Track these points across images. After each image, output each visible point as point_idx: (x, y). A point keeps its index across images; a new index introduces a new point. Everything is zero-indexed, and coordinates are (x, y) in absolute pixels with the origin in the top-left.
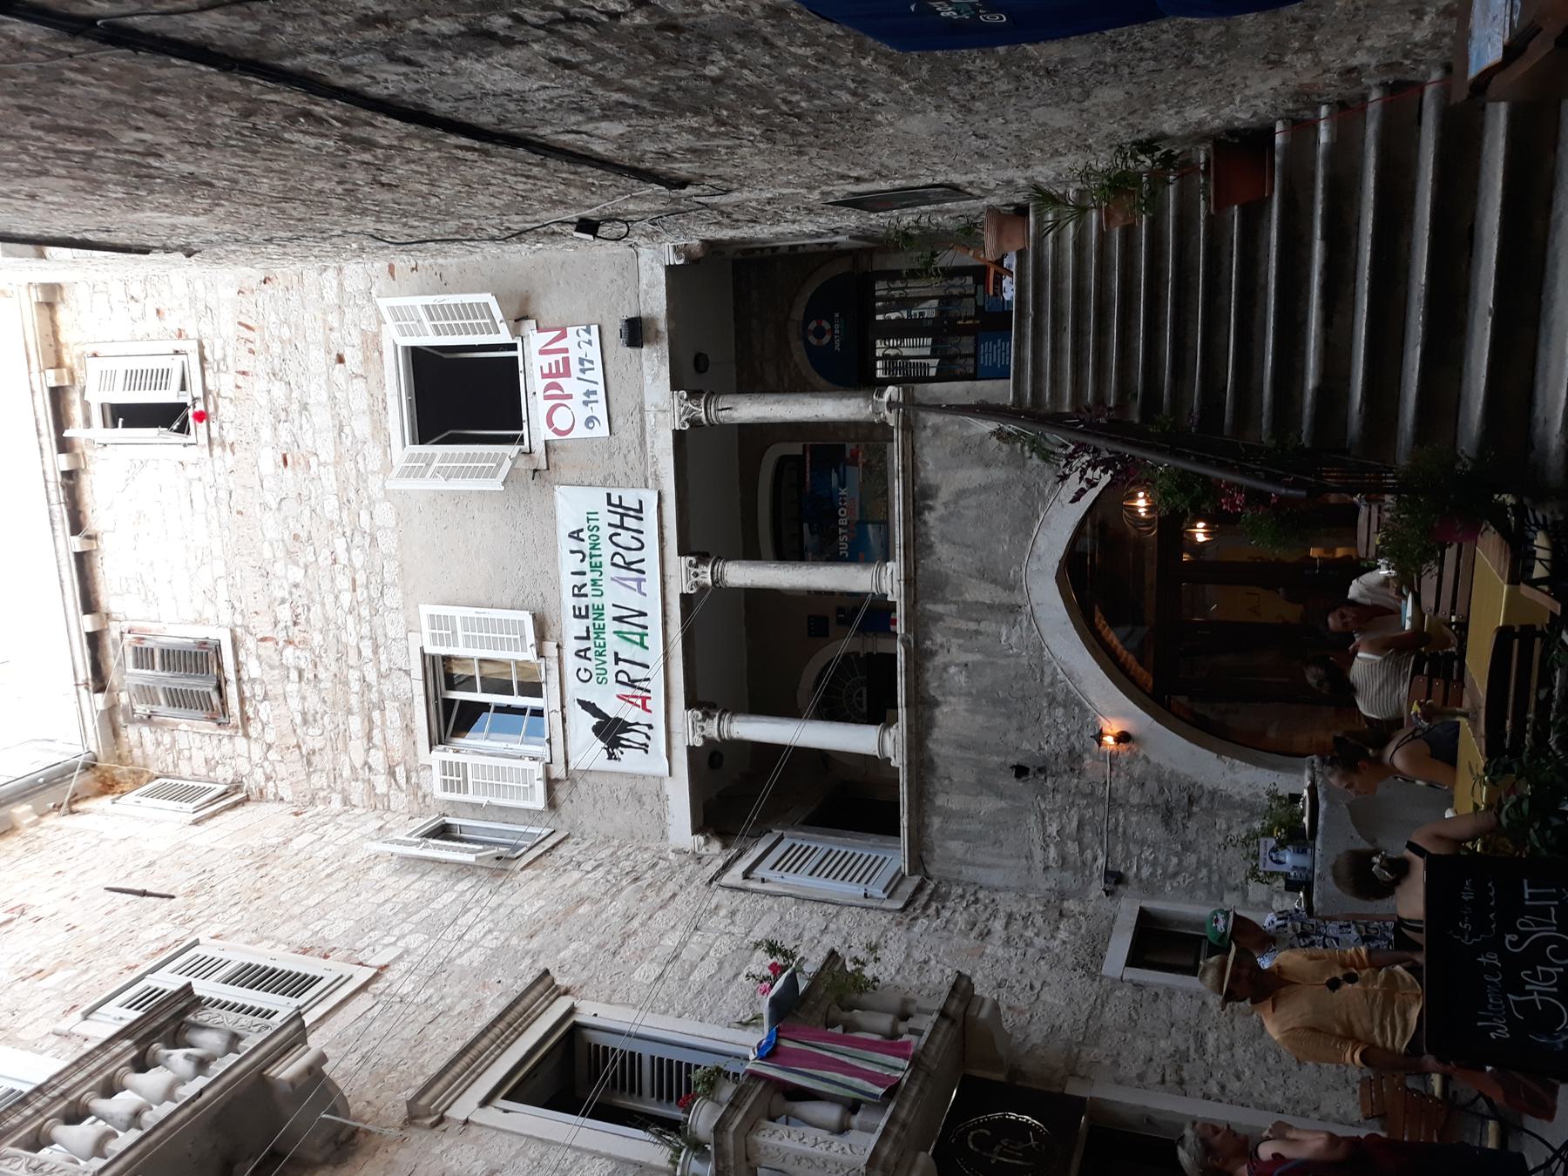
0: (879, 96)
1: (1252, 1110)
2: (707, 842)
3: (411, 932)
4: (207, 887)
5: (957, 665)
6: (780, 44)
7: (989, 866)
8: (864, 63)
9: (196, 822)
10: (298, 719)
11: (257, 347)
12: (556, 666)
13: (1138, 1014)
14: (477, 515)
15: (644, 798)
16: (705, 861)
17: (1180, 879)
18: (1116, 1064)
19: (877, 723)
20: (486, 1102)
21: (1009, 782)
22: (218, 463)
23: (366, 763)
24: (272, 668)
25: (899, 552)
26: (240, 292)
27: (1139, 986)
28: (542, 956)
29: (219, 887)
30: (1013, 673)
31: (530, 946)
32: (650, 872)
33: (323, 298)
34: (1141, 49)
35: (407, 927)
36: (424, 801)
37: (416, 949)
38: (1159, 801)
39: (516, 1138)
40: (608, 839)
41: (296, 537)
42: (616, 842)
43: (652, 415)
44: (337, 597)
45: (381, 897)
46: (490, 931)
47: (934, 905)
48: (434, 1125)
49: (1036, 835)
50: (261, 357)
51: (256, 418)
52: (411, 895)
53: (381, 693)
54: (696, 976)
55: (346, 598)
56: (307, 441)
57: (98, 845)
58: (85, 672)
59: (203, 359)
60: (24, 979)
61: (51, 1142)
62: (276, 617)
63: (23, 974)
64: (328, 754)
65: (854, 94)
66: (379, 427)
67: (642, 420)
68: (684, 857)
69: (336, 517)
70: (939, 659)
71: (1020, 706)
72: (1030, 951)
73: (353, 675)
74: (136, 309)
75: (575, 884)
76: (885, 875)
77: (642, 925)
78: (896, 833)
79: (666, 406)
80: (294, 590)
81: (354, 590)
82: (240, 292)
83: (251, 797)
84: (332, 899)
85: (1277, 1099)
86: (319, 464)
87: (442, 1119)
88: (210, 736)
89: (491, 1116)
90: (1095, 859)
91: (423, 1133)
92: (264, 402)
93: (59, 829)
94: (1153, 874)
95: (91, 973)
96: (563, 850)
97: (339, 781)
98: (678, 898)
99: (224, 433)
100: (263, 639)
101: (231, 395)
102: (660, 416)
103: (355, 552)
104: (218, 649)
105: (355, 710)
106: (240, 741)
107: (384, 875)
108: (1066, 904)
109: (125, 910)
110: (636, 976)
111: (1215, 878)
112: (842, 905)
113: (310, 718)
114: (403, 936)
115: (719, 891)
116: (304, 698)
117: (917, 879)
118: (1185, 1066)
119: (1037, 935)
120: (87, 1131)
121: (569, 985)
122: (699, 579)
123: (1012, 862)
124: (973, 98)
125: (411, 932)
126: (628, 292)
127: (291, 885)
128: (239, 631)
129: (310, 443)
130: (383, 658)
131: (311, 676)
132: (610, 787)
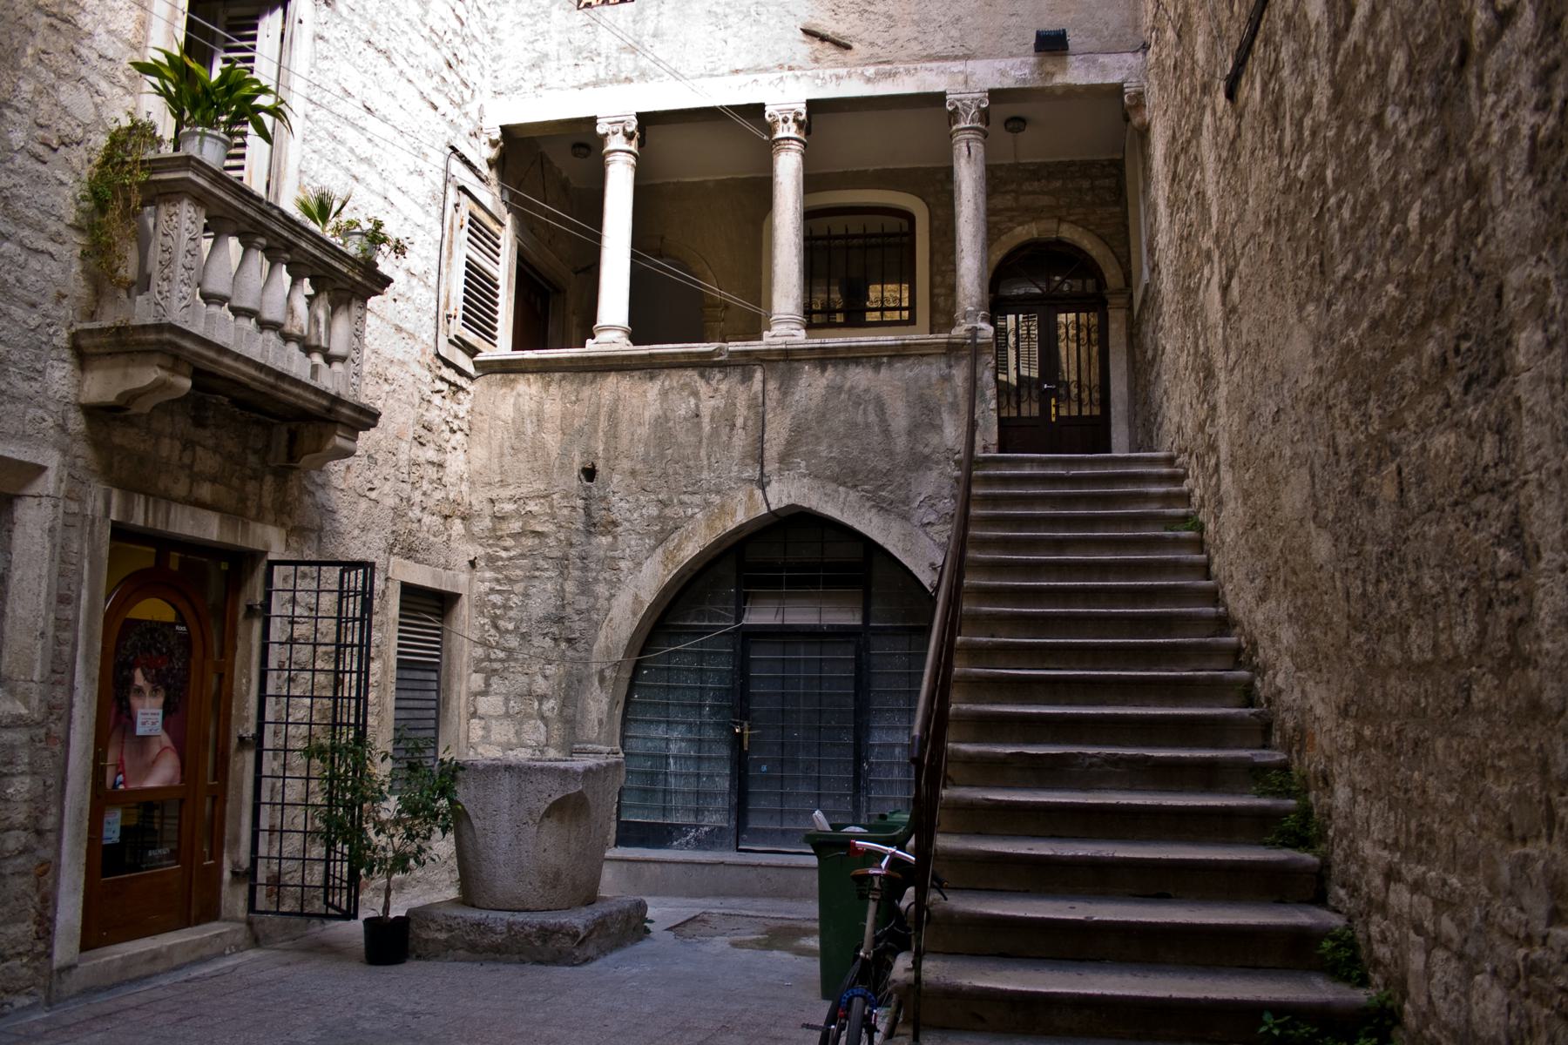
0: (1340, 307)
2: (493, 144)
5: (697, 406)
6: (1427, 191)
8: (1390, 288)
15: (537, 71)
16: (473, 140)
17: (493, 632)
19: (630, 324)
21: (577, 463)
25: (816, 343)
30: (691, 463)
32: (457, 81)
34: (1378, 581)
38: (569, 610)
43: (961, 67)
47: (445, 387)
49: (524, 490)
65: (1346, 278)
67: (956, 58)
70: (701, 385)
71: (658, 472)
72: (408, 487)
78: (514, 349)
90: (506, 549)
94: (494, 606)
98: (433, 111)
102: (961, 78)
108: (458, 521)
111: (497, 665)
117: (471, 369)
119: (424, 494)
122: (781, 124)
123: (495, 467)
124: (1329, 408)
132: (548, 32)
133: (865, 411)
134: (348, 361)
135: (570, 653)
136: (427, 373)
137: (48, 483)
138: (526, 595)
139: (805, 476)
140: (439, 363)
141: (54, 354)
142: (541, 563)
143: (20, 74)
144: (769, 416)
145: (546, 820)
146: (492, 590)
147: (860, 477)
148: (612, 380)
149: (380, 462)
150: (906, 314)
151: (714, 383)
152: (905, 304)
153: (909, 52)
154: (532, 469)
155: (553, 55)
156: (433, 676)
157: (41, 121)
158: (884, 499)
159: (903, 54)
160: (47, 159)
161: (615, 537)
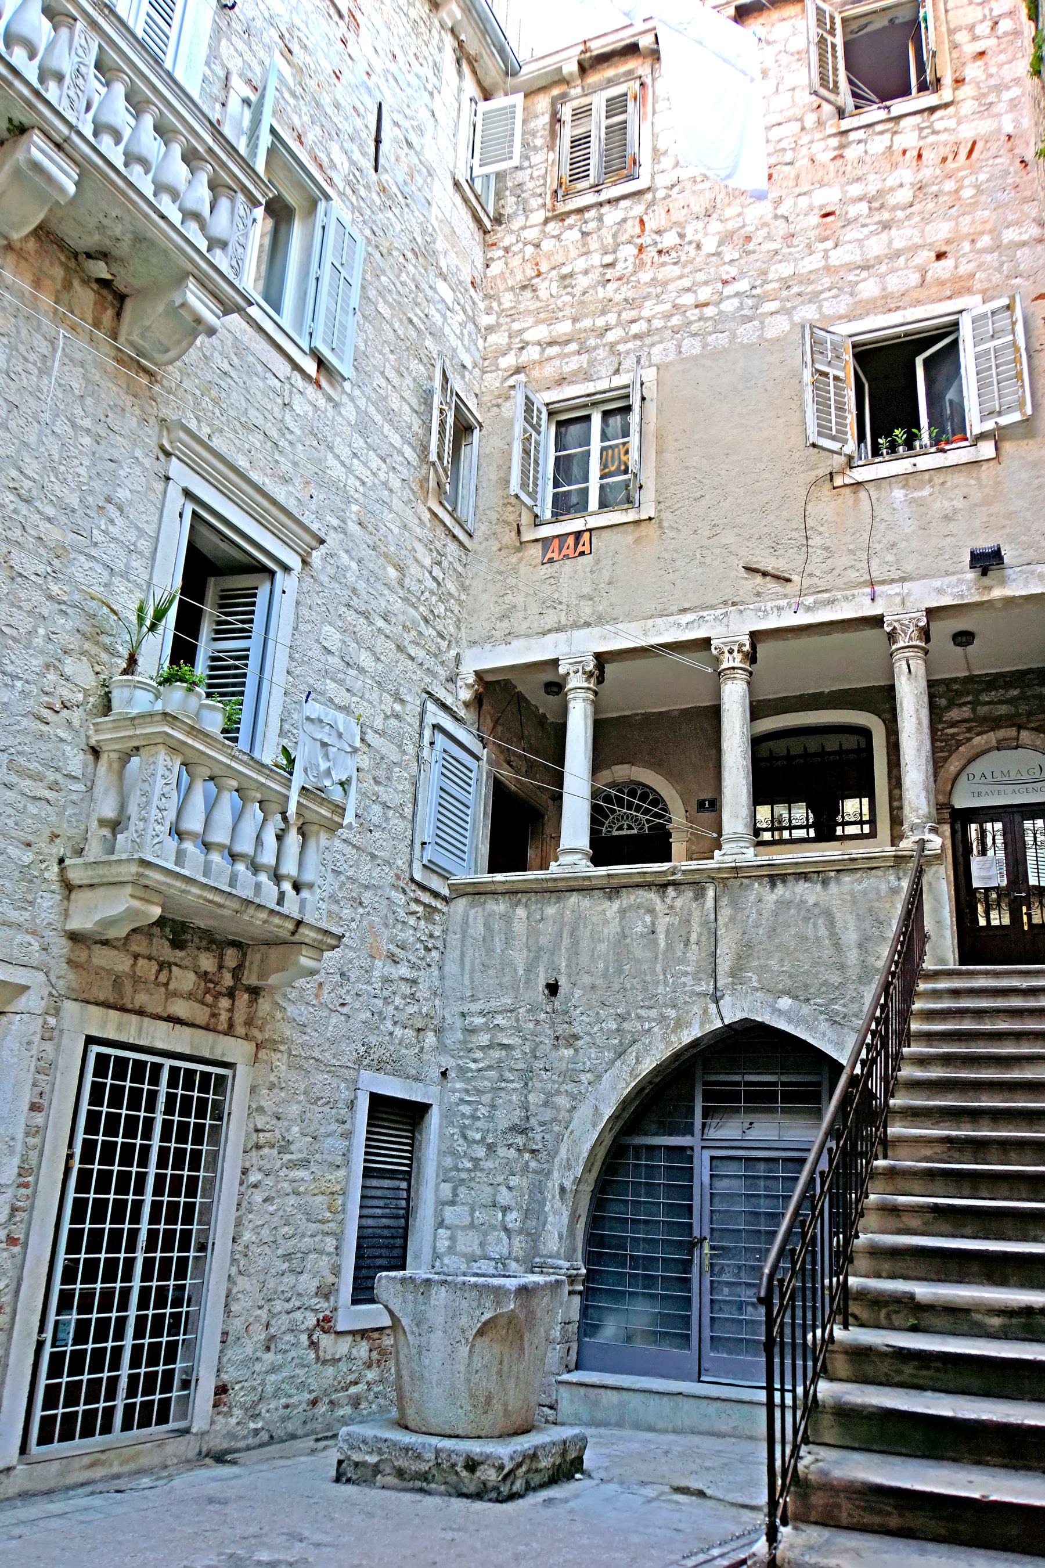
1: (234, 1214)
2: (469, 686)
3: (357, 407)
4: (389, 203)
5: (653, 923)
7: (462, 960)
9: (457, 184)
10: (565, 270)
11: (950, 165)
12: (631, 519)
13: (323, 1105)
14: (782, 420)
16: (450, 686)
17: (461, 1141)
18: (272, 1087)
20: (188, 494)
22: (821, 145)
23: (527, 343)
24: (615, 236)
26: (1010, 137)
27: (352, 1105)
28: (342, 536)
29: (390, 214)
30: (648, 978)
31: (350, 523)
32: (434, 633)
33: (1008, 227)
35: (362, 403)
36: (493, 406)
37: (340, 413)
39: (155, 526)
40: (464, 588)
41: (748, 239)
42: (463, 597)
43: (898, 590)
44: (689, 290)
45: (391, 374)
46: (363, 483)
47: (420, 909)
48: (162, 448)
50: (938, 171)
51: (871, 177)
52: (395, 403)
53: (595, 348)
54: (331, 685)
55: (688, 299)
56: (853, 234)
57: (425, 89)
58: (598, 47)
59: (932, 110)
60: (282, 37)
61: (108, 84)
62: (665, 231)
63: (287, 36)
64: (533, 305)
66: (869, 307)
67: (893, 581)
68: (452, 665)
69: (771, 276)
70: (659, 907)
71: (616, 987)
72: (379, 1003)
73: (612, 318)
74: (984, 29)
75: (417, 561)
76: (444, 861)
77: (379, 630)
78: (492, 870)
79: (908, 604)
80: (694, 245)
81: (697, 306)
82: (1010, 137)
83: (488, 236)
84: (386, 327)
85: (247, 1236)
86: (826, 251)
87: (168, 454)
88: (544, 185)
89: (175, 500)
90: (475, 1061)
91: (155, 439)
92: (890, 182)
93: (440, 50)
94: (463, 1115)
95: (292, 101)
96: (452, 547)
97: (508, 320)
98: (410, 662)
99: (854, 145)
100: (642, 222)
101: (895, 147)
102: (898, 599)
103: (736, 302)
104: (631, 177)
105: (578, 326)
106: (539, 216)
107: (414, 374)
108: (431, 1034)
109: (359, 123)
110: (327, 629)
111: (464, 1175)
112: (413, 821)
113: (568, 281)
114: (352, 399)
115: (418, 703)
116: (586, 272)
117: (446, 892)
118: (275, 1151)
119: (396, 1008)
120: (120, 114)
121: (314, 565)
123: (467, 982)
125: (357, 407)
126: (1031, 552)
127: (398, 285)
128: (649, 196)
129: (847, 238)
130: (630, 345)
131: (608, 277)
133: (815, 925)
134: (316, 887)
135: (533, 1164)
136: (401, 896)
137: (33, 1001)
138: (493, 1107)
139: (757, 990)
140: (414, 887)
141: (44, 887)
142: (508, 1075)
143: (31, 652)
144: (721, 932)
145: (479, 1340)
146: (461, 1100)
147: (812, 990)
148: (574, 899)
149: (352, 979)
150: (866, 829)
151: (668, 900)
152: (866, 818)
153: (845, 580)
154: (500, 984)
155: (520, 606)
156: (404, 1185)
157: (46, 689)
158: (837, 1013)
159: (840, 582)
160: (50, 720)
161: (576, 1050)
